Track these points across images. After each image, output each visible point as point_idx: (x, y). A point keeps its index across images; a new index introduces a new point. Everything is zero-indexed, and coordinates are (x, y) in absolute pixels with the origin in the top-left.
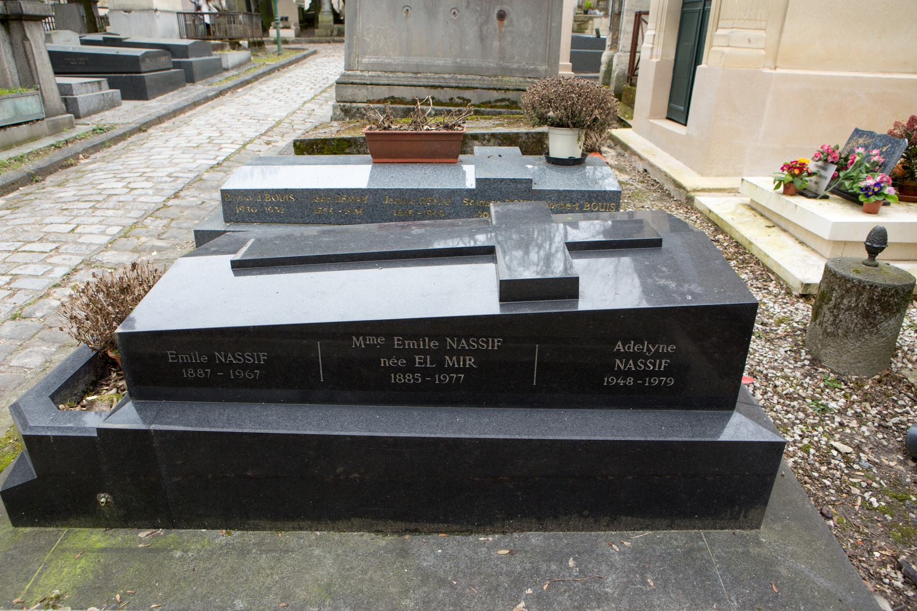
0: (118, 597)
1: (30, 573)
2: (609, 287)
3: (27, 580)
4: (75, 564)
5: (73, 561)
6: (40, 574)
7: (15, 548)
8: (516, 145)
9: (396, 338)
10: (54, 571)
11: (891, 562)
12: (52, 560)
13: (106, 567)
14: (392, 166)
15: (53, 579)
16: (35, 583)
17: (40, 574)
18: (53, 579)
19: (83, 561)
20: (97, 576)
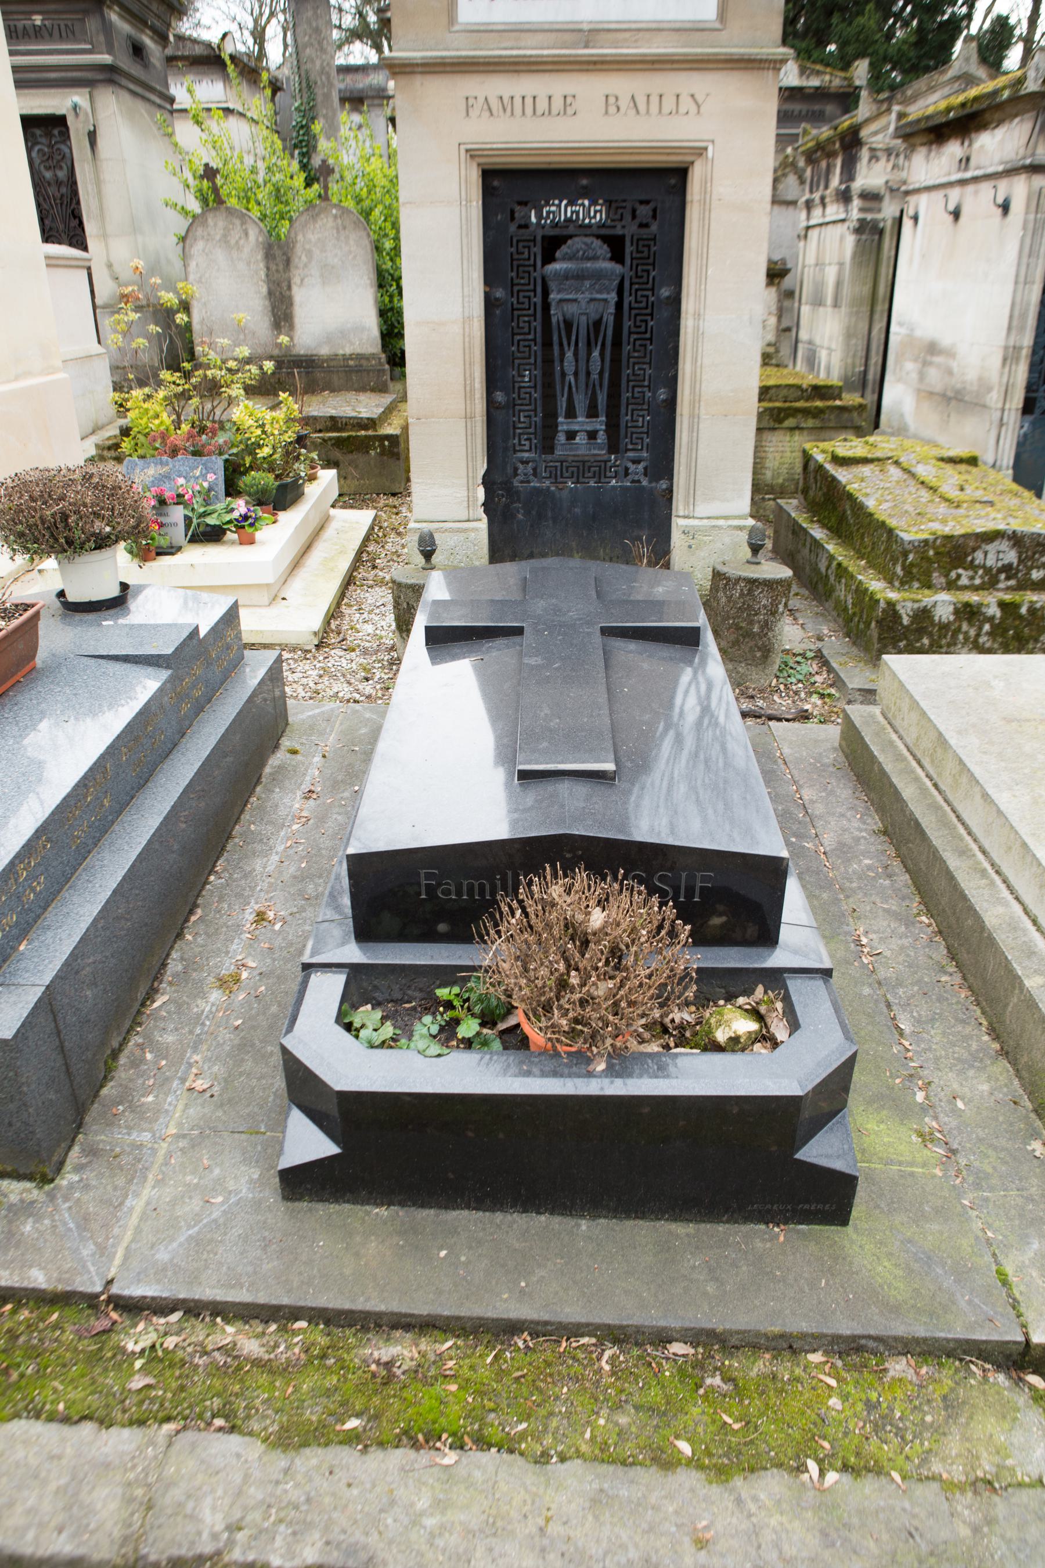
0: (898, 1081)
1: (903, 1175)
2: (193, 918)
3: (912, 1174)
4: (876, 1133)
5: (872, 1137)
6: (900, 1164)
7: (877, 1207)
8: (16, 1036)
9: (699, 875)
10: (892, 1150)
11: (944, 627)
12: (881, 1158)
13: (870, 1102)
14: (575, 75)
15: (902, 1147)
16: (912, 1164)
17: (900, 1164)
18: (902, 1147)
19: (869, 1126)
20: (883, 1107)
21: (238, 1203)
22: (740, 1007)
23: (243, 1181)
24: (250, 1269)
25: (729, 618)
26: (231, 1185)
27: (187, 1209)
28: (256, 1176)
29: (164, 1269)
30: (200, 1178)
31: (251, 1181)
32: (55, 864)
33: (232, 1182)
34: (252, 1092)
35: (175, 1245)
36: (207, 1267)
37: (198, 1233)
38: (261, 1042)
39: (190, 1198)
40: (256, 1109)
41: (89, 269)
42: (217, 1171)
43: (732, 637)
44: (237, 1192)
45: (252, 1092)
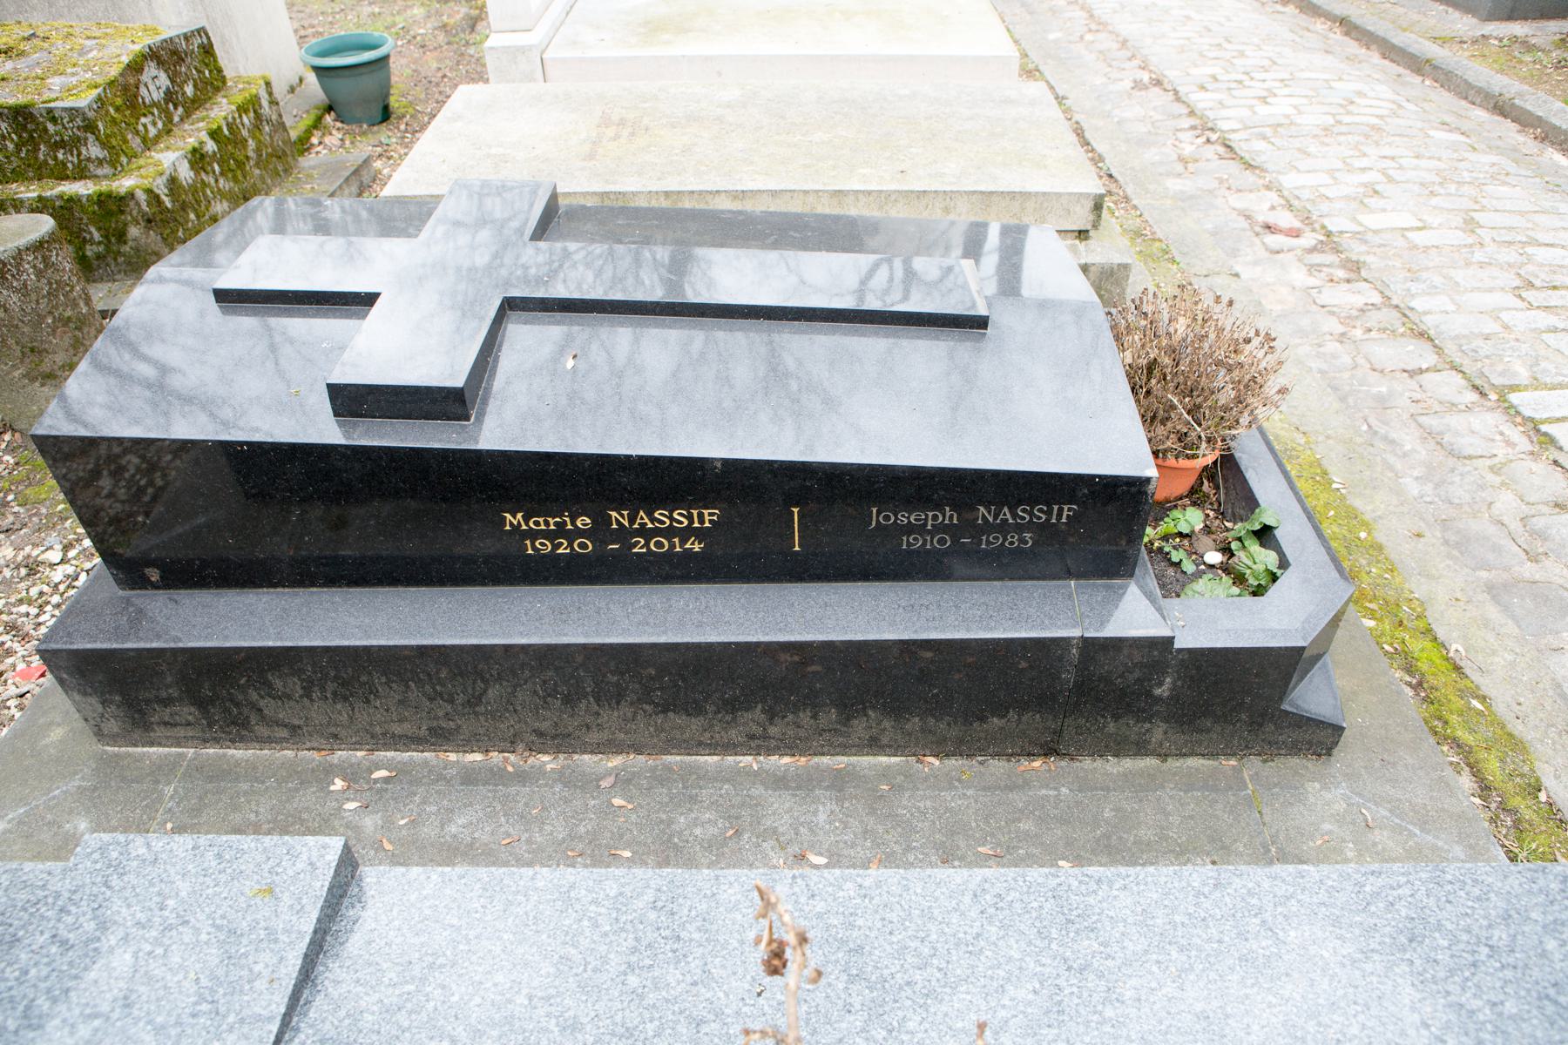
21: (1359, 795)
22: (1192, 113)
23: (1328, 796)
24: (1421, 773)
25: (42, 318)
26: (1341, 806)
27: (1391, 844)
28: (1317, 785)
29: (1471, 847)
30: (1344, 841)
31: (1325, 787)
32: (1340, 992)
33: (1336, 806)
34: (1191, 817)
35: (1440, 844)
36: (1443, 810)
37: (1415, 825)
38: (1099, 826)
39: (1375, 844)
40: (1219, 806)
41: (511, 305)
42: (1327, 826)
43: (67, 340)
44: (1345, 798)
45: (1191, 817)
